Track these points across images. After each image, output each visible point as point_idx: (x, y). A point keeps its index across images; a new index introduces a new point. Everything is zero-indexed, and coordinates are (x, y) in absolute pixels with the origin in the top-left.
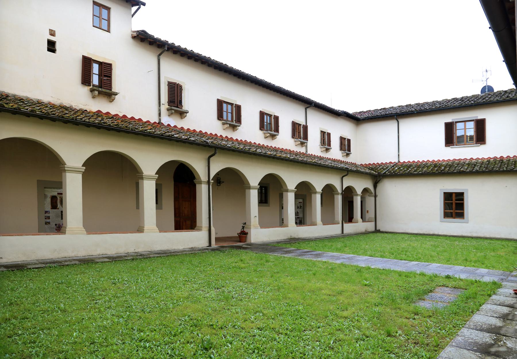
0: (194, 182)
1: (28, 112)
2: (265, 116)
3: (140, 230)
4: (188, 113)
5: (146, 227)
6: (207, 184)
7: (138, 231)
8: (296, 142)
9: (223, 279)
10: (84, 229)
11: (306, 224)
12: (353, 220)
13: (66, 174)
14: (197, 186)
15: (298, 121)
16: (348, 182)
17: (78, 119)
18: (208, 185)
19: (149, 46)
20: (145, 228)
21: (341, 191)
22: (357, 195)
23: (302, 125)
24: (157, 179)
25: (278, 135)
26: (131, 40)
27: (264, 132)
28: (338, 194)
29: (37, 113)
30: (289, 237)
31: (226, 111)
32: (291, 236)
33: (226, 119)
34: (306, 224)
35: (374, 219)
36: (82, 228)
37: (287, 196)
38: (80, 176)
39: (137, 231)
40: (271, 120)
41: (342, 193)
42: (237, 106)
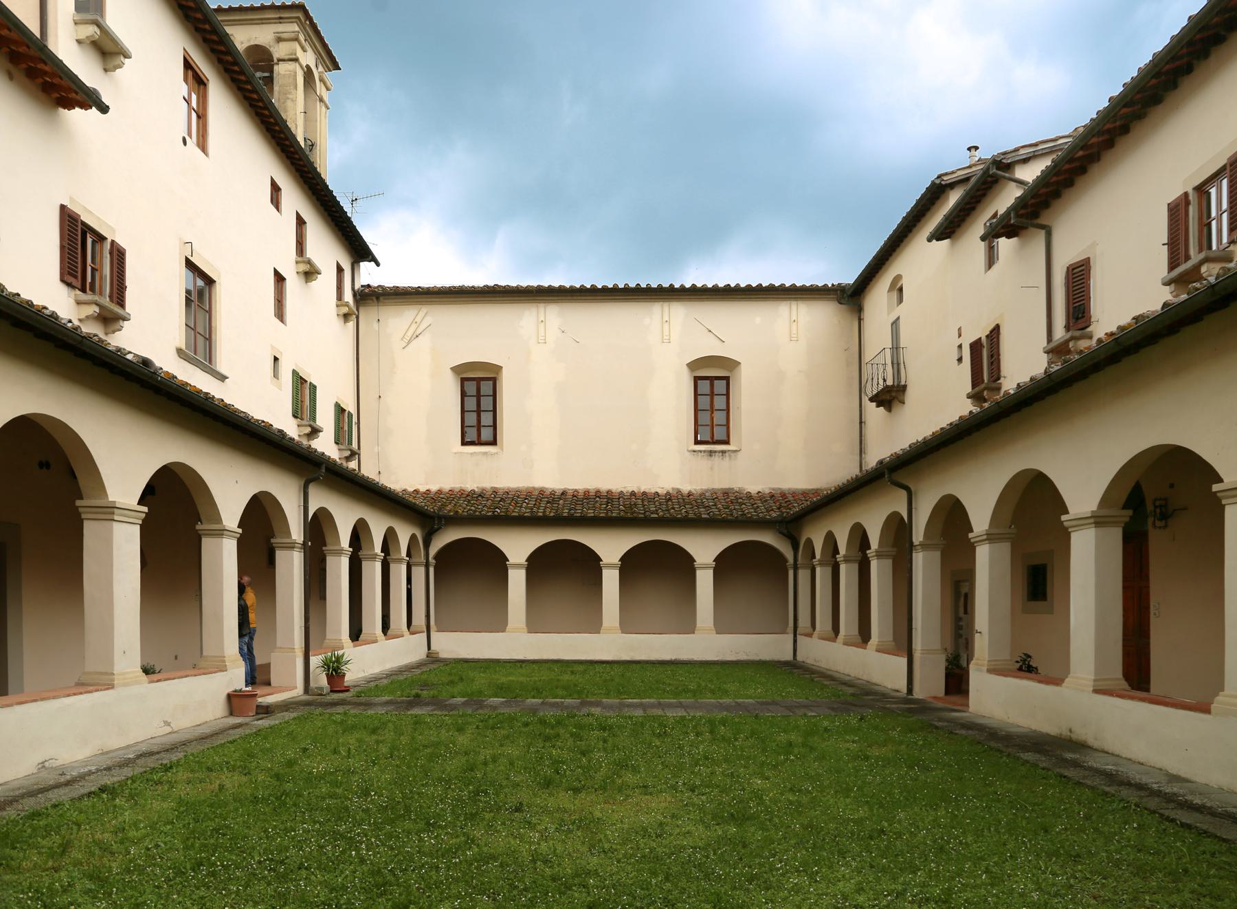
0: (358, 556)
3: (104, 682)
6: (301, 548)
7: (80, 684)
9: (836, 807)
13: (112, 527)
14: (207, 543)
16: (320, 499)
19: (285, 158)
21: (299, 536)
22: (221, 533)
23: (109, 240)
26: (892, 412)
27: (75, 295)
28: (291, 546)
30: (1065, 733)
32: (1070, 731)
37: (108, 542)
39: (73, 684)
41: (304, 544)
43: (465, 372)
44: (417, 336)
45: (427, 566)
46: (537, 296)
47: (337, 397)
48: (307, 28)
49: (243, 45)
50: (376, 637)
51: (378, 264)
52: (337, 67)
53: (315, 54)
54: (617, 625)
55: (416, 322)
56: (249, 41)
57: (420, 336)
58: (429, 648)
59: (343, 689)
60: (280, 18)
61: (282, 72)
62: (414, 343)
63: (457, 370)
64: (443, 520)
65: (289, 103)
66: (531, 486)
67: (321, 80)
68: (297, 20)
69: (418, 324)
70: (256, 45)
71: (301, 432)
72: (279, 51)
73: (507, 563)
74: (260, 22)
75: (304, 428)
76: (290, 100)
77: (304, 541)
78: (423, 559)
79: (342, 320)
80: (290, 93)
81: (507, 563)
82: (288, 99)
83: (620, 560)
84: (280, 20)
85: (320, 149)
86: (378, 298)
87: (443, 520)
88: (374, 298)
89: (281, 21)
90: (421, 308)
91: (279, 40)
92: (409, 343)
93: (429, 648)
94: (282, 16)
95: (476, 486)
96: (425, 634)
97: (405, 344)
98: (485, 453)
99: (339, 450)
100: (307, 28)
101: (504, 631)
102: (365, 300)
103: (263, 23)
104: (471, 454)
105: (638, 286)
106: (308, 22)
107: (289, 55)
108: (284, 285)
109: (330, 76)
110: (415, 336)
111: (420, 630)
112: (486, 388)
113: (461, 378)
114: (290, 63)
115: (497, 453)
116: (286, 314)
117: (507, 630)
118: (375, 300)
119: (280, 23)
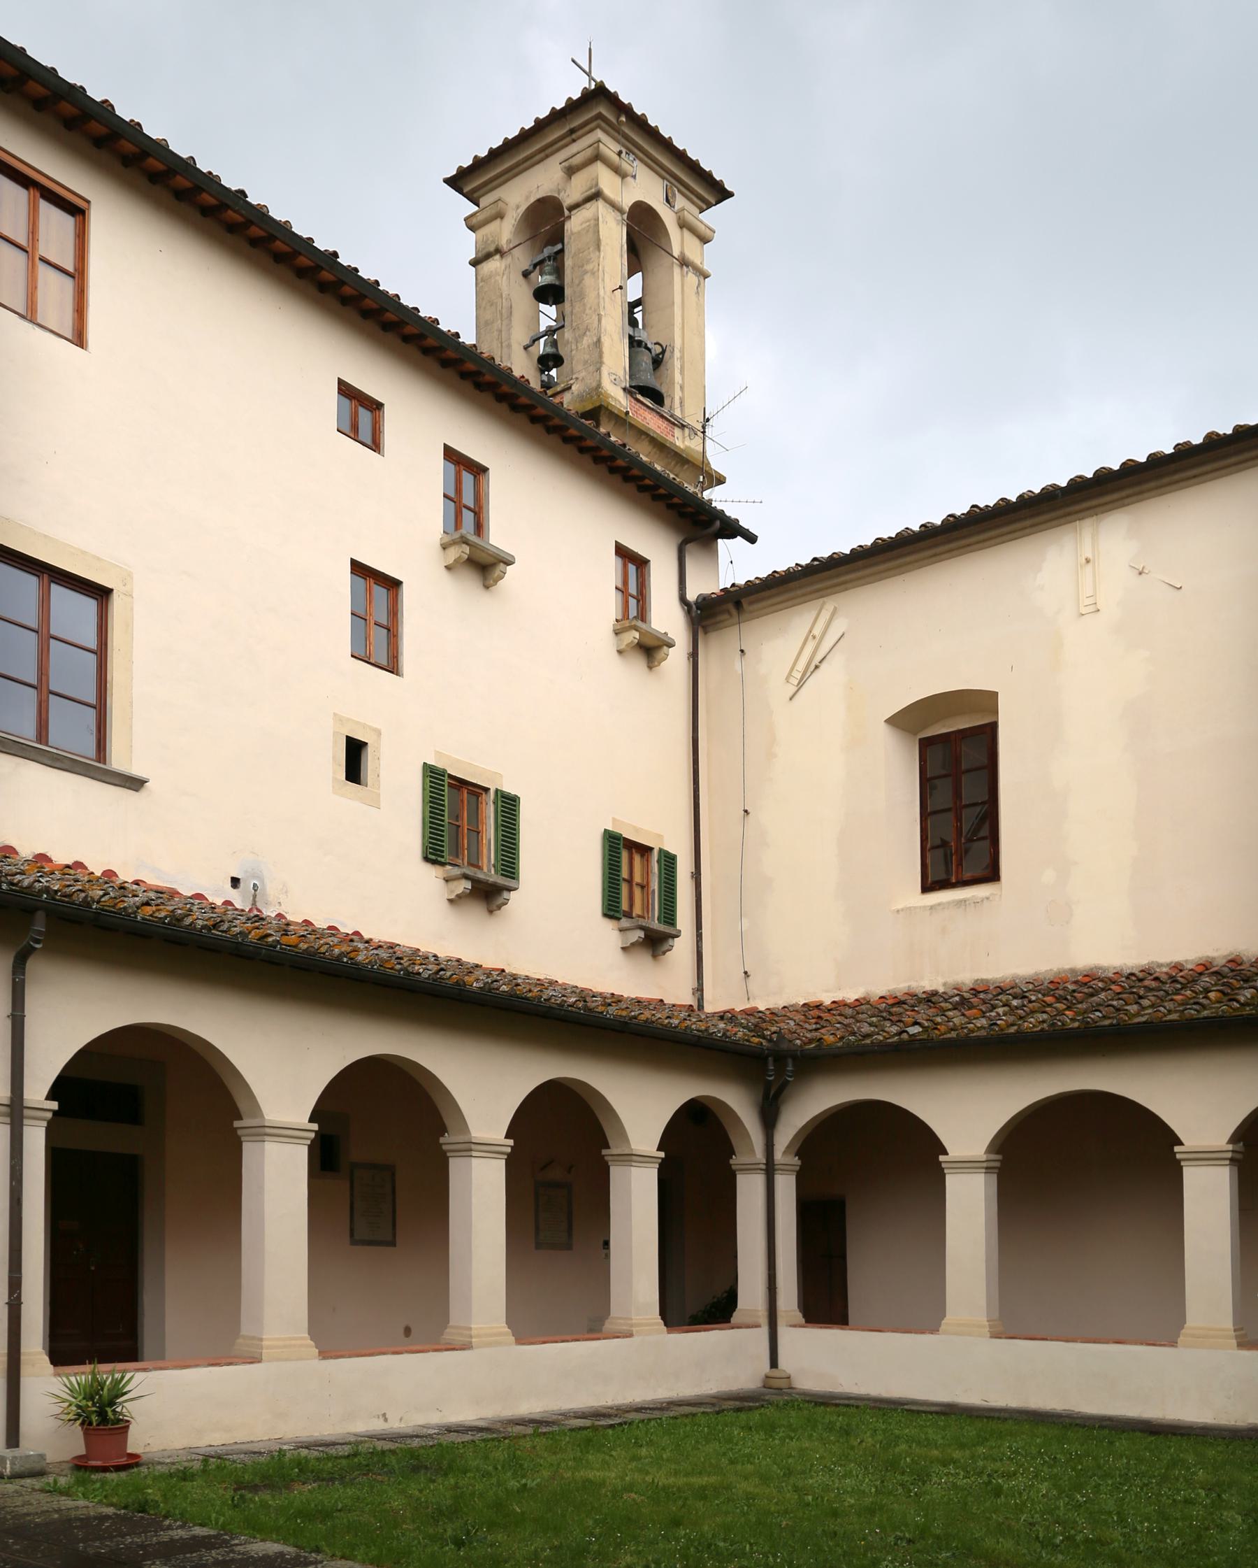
1: (153, 921)
2: (625, 855)
4: (677, 936)
5: (269, 1347)
8: (453, 885)
10: (312, 1342)
11: (162, 1357)
12: (608, 1326)
15: (637, 830)
17: (494, 989)
18: (8, 1128)
20: (265, 1343)
24: (509, 1155)
25: (515, 889)
29: (213, 934)
31: (93, 700)
33: (92, 752)
34: (162, 1357)
35: (764, 1320)
36: (504, 1327)
38: (500, 1165)
40: (647, 872)
42: (503, 797)
43: (925, 727)
44: (817, 667)
45: (770, 1170)
46: (1068, 505)
47: (614, 820)
48: (627, 131)
49: (519, 211)
50: (471, 1337)
51: (752, 539)
52: (722, 193)
53: (663, 178)
54: (1228, 1323)
55: (814, 637)
56: (527, 198)
57: (823, 666)
58: (774, 1363)
59: (123, 1461)
60: (572, 131)
61: (575, 230)
62: (811, 682)
63: (903, 721)
64: (790, 1061)
65: (588, 280)
66: (1067, 967)
67: (683, 225)
68: (599, 122)
69: (818, 638)
70: (539, 200)
71: (452, 892)
72: (573, 192)
73: (942, 1158)
74: (542, 155)
75: (455, 883)
76: (589, 274)
77: (12, 1099)
78: (759, 1155)
79: (639, 662)
80: (588, 261)
81: (942, 1158)
82: (586, 272)
83: (1234, 1139)
84: (572, 135)
85: (682, 358)
86: (738, 605)
87: (790, 1061)
88: (731, 606)
89: (574, 136)
90: (824, 603)
91: (571, 171)
92: (801, 684)
93: (774, 1363)
94: (572, 126)
95: (941, 980)
96: (764, 1332)
97: (793, 689)
98: (961, 903)
99: (621, 930)
100: (627, 131)
101: (934, 1330)
102: (713, 615)
103: (547, 156)
104: (932, 908)
105: (507, 142)
106: (623, 119)
107: (586, 191)
108: (400, 594)
109: (714, 217)
110: (812, 667)
111: (749, 1321)
112: (971, 755)
113: (921, 741)
114: (588, 205)
115: (988, 898)
116: (402, 654)
117: (943, 1328)
118: (734, 612)
119: (574, 141)
